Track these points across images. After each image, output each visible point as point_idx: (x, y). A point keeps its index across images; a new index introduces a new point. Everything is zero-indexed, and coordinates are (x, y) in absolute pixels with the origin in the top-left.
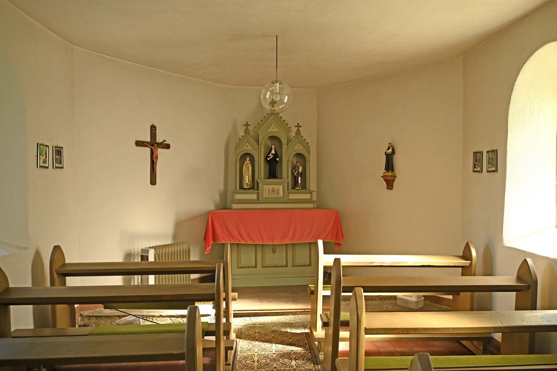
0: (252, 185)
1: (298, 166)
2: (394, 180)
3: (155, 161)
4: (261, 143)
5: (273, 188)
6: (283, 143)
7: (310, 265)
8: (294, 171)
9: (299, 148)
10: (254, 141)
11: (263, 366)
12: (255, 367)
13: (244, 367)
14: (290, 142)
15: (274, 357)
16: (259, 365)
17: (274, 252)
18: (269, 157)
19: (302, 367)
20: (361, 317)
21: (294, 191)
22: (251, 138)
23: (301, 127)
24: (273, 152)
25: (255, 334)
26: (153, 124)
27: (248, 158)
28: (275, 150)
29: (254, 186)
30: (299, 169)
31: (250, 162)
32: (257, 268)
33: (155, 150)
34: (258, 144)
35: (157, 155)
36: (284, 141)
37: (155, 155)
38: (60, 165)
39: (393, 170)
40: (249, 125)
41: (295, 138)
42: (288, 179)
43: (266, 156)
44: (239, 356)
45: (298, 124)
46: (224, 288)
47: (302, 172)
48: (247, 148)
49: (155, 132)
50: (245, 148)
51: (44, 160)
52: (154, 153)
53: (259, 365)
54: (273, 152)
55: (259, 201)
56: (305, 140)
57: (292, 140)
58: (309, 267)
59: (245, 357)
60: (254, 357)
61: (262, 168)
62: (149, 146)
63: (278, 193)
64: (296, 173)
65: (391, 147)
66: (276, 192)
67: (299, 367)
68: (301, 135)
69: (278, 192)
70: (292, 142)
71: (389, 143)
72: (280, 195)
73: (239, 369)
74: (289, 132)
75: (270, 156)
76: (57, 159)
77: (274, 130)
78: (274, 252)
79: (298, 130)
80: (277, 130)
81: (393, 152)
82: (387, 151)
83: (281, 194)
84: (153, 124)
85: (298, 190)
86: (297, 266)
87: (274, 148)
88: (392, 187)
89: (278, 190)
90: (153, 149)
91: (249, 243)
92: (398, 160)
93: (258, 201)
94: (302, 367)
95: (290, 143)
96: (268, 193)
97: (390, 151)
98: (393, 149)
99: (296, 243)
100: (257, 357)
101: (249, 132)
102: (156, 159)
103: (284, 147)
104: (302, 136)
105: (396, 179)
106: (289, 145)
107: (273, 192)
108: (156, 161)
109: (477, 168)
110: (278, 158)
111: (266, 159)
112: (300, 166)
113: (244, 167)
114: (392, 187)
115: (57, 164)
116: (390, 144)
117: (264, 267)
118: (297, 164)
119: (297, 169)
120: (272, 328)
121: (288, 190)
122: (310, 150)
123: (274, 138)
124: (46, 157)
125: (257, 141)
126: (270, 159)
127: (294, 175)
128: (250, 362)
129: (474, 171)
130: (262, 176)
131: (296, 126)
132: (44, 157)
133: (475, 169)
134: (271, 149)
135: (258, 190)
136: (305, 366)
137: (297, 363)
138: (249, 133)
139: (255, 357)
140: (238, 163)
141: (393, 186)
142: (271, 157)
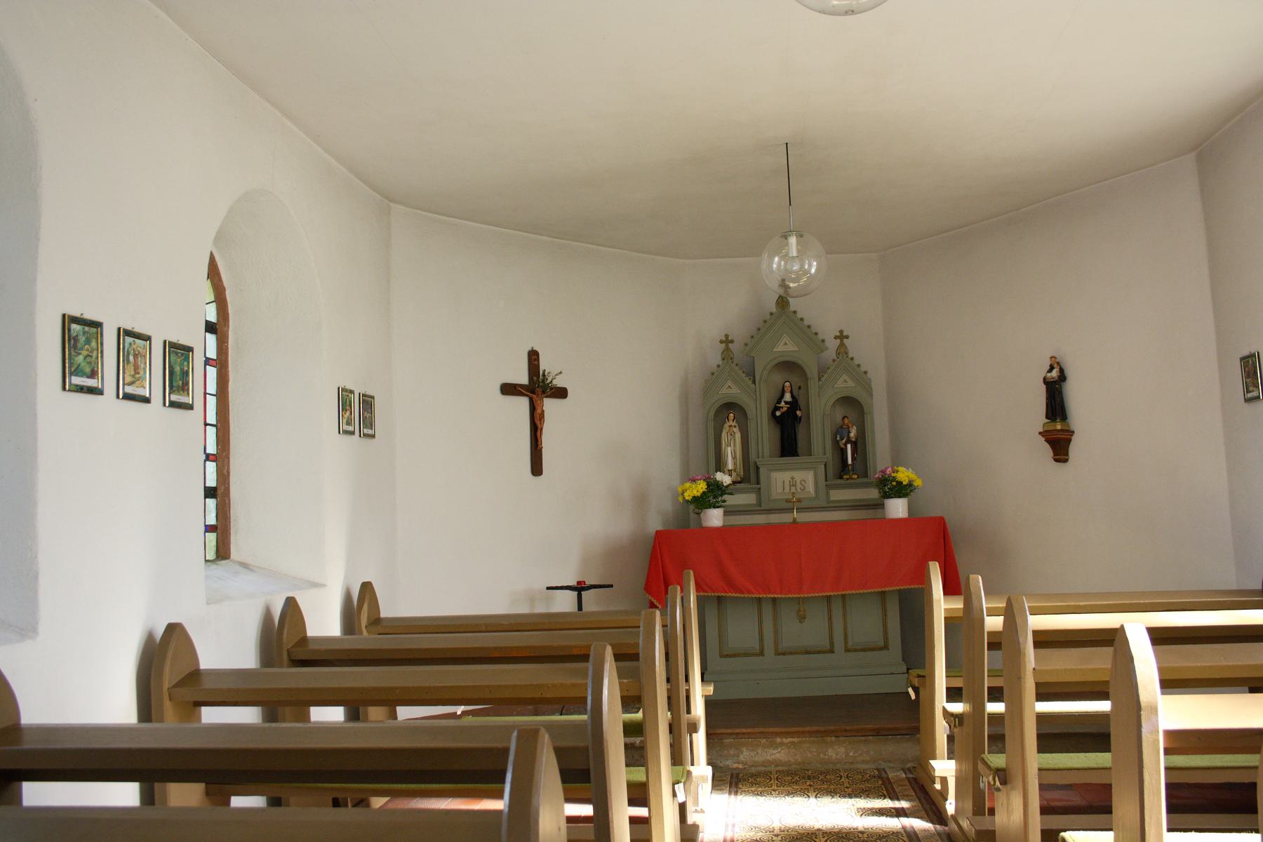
0: (742, 474)
1: (848, 426)
2: (1069, 441)
3: (539, 425)
4: (761, 378)
5: (793, 478)
6: (749, 417)
7: (886, 647)
8: (838, 438)
9: (844, 384)
10: (744, 375)
14: (825, 372)
17: (802, 618)
18: (777, 408)
20: (1025, 648)
21: (840, 481)
22: (737, 368)
23: (847, 337)
24: (788, 397)
26: (532, 348)
27: (732, 415)
28: (791, 392)
29: (750, 476)
30: (850, 432)
31: (737, 422)
32: (764, 656)
33: (539, 402)
34: (754, 382)
35: (543, 411)
36: (812, 371)
37: (539, 411)
38: (370, 432)
39: (1064, 417)
40: (732, 342)
41: (836, 362)
42: (825, 454)
43: (773, 407)
45: (841, 332)
47: (857, 439)
48: (731, 391)
49: (536, 363)
50: (724, 390)
51: (348, 418)
52: (536, 407)
54: (788, 397)
55: (762, 508)
56: (859, 366)
57: (828, 368)
58: (884, 652)
61: (765, 434)
62: (527, 393)
63: (804, 489)
64: (844, 441)
65: (1055, 366)
66: (799, 486)
68: (850, 356)
69: (803, 486)
70: (829, 371)
71: (1051, 358)
72: (809, 492)
74: (822, 352)
75: (782, 407)
76: (366, 417)
77: (786, 347)
78: (802, 618)
79: (842, 344)
80: (791, 347)
81: (1062, 377)
82: (1049, 375)
83: (811, 490)
84: (532, 348)
85: (847, 479)
86: (855, 650)
87: (789, 389)
88: (1066, 457)
89: (803, 482)
90: (534, 400)
91: (746, 596)
92: (1076, 396)
93: (759, 508)
95: (826, 376)
96: (780, 491)
97: (1055, 373)
98: (1062, 371)
99: (850, 592)
101: (732, 356)
102: (540, 420)
103: (813, 386)
104: (852, 359)
105: (1073, 438)
106: (823, 379)
107: (793, 485)
108: (541, 424)
109: (1252, 391)
110: (800, 410)
111: (773, 414)
112: (853, 425)
113: (724, 434)
114: (1066, 457)
115: (366, 428)
116: (1053, 359)
117: (779, 654)
118: (843, 422)
119: (845, 433)
120: (812, 783)
121: (826, 481)
122: (871, 388)
123: (789, 366)
124: (351, 414)
125: (751, 374)
126: (783, 414)
127: (839, 446)
129: (1247, 400)
130: (767, 452)
131: (836, 338)
132: (348, 413)
133: (1249, 395)
134: (783, 392)
135: (758, 483)
138: (732, 359)
140: (711, 424)
141: (1067, 454)
142: (785, 409)
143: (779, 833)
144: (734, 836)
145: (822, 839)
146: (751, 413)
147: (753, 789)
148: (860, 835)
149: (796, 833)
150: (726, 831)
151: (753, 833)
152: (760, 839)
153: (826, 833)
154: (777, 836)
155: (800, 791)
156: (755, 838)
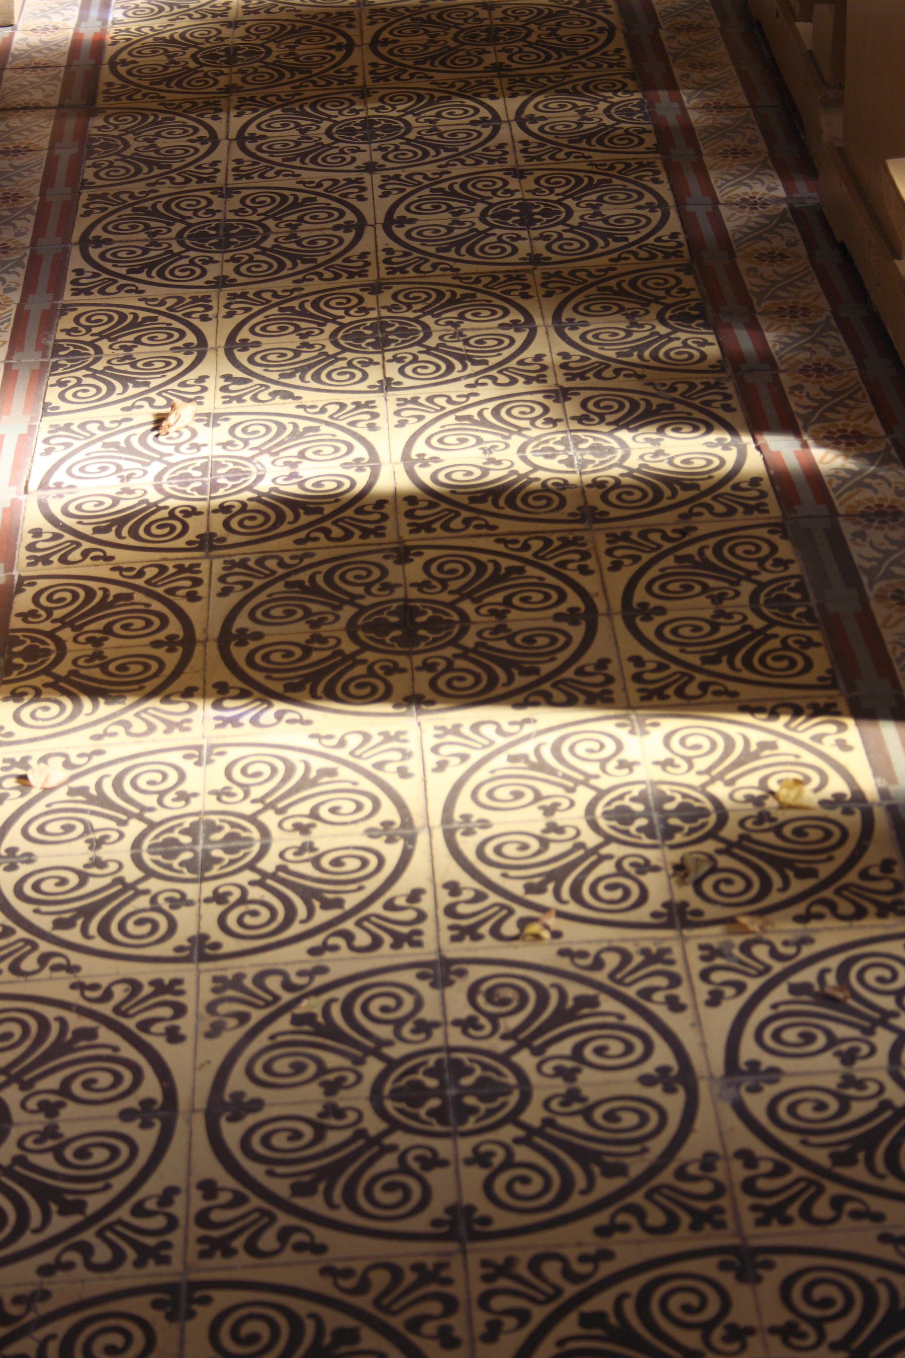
11: (531, 571)
12: (421, 916)
13: (328, 577)
15: (418, 660)
16: (354, 435)
19: (526, 547)
25: (50, 473)
44: (30, 592)
46: (410, 847)
53: (354, 435)
59: (91, 594)
60: (193, 597)
67: (548, 542)
73: (232, 539)
94: (526, 547)
100: (441, 766)
128: (141, 646)
136: (746, 674)
137: (647, 655)
139: (201, 590)
143: (241, 17)
144: (104, 31)
145: (366, 28)
146: (118, 1273)
147: (456, 389)
148: (483, 14)
149: (291, 16)
150: (82, 18)
151: (164, 21)
152: (182, 36)
153: (383, 10)
154: (233, 25)
155: (621, 176)
156: (167, 35)
